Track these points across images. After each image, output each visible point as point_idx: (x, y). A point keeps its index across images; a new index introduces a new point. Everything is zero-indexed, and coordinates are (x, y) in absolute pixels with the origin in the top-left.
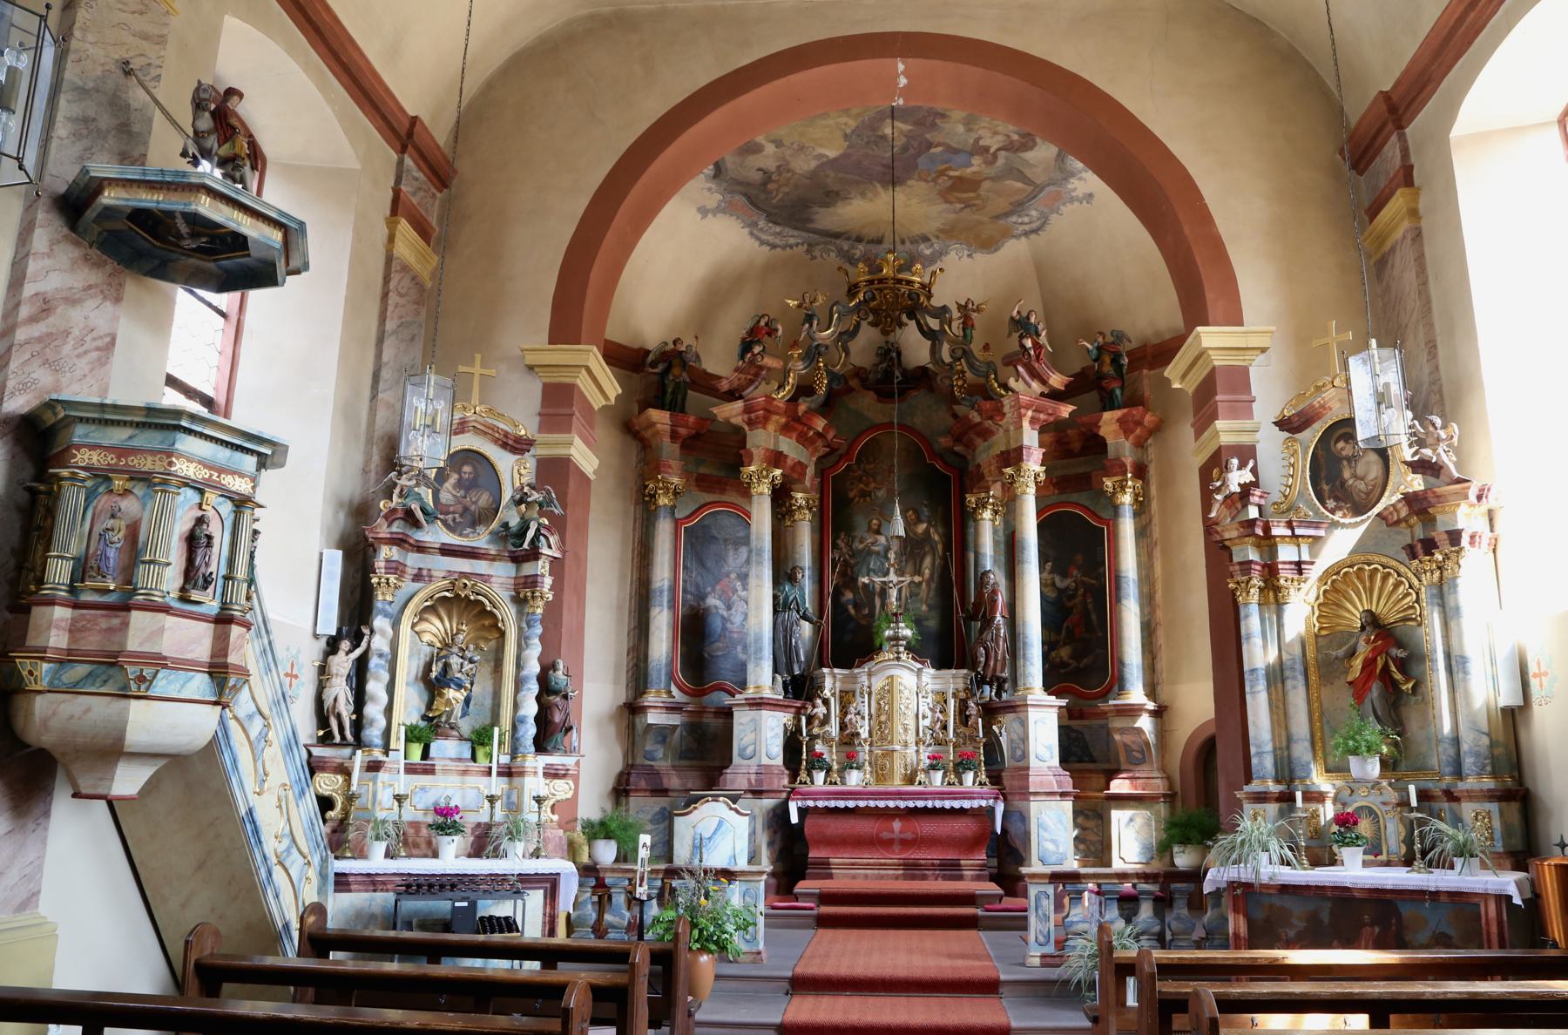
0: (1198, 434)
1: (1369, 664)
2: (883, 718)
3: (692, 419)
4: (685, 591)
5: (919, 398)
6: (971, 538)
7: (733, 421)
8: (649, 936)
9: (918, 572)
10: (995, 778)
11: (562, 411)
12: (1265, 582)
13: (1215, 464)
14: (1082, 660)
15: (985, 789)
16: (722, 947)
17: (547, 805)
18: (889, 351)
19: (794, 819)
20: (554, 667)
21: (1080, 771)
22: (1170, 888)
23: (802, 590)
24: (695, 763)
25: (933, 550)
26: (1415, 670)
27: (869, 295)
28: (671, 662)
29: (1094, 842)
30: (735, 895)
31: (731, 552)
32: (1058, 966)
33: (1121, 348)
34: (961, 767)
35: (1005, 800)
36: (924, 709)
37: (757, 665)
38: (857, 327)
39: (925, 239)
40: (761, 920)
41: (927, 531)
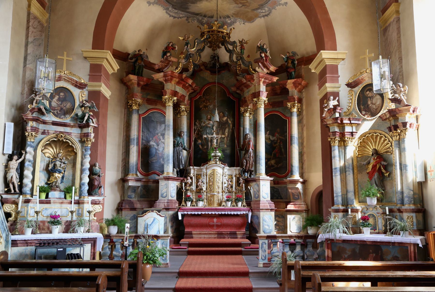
0: (320, 88)
1: (374, 167)
2: (211, 184)
3: (145, 79)
4: (142, 139)
5: (225, 74)
6: (242, 123)
7: (160, 80)
8: (128, 259)
9: (224, 134)
10: (249, 204)
11: (97, 74)
12: (340, 139)
13: (325, 98)
14: (278, 164)
15: (245, 208)
16: (155, 262)
17: (92, 214)
18: (215, 57)
19: (180, 218)
20: (95, 165)
21: (277, 202)
22: (306, 241)
23: (183, 139)
24: (146, 199)
25: (229, 126)
26: (389, 169)
27: (208, 36)
28: (137, 164)
29: (281, 225)
30: (159, 244)
31: (159, 126)
32: (269, 267)
33: (295, 58)
34: (237, 200)
35: (252, 211)
36: (225, 181)
37: (168, 165)
38: (204, 48)
39: (228, 17)
40: (168, 253)
41: (227, 120)
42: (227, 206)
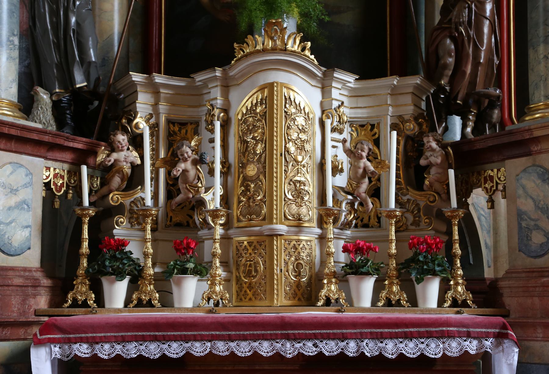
2: (252, 170)
15: (466, 315)
34: (411, 271)
36: (336, 153)
42: (350, 301)
